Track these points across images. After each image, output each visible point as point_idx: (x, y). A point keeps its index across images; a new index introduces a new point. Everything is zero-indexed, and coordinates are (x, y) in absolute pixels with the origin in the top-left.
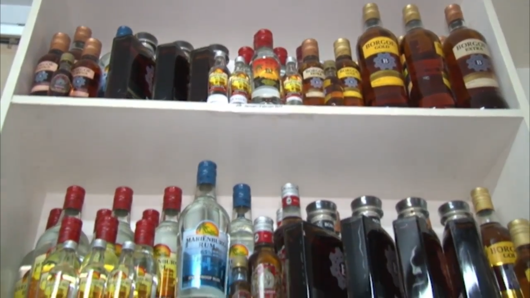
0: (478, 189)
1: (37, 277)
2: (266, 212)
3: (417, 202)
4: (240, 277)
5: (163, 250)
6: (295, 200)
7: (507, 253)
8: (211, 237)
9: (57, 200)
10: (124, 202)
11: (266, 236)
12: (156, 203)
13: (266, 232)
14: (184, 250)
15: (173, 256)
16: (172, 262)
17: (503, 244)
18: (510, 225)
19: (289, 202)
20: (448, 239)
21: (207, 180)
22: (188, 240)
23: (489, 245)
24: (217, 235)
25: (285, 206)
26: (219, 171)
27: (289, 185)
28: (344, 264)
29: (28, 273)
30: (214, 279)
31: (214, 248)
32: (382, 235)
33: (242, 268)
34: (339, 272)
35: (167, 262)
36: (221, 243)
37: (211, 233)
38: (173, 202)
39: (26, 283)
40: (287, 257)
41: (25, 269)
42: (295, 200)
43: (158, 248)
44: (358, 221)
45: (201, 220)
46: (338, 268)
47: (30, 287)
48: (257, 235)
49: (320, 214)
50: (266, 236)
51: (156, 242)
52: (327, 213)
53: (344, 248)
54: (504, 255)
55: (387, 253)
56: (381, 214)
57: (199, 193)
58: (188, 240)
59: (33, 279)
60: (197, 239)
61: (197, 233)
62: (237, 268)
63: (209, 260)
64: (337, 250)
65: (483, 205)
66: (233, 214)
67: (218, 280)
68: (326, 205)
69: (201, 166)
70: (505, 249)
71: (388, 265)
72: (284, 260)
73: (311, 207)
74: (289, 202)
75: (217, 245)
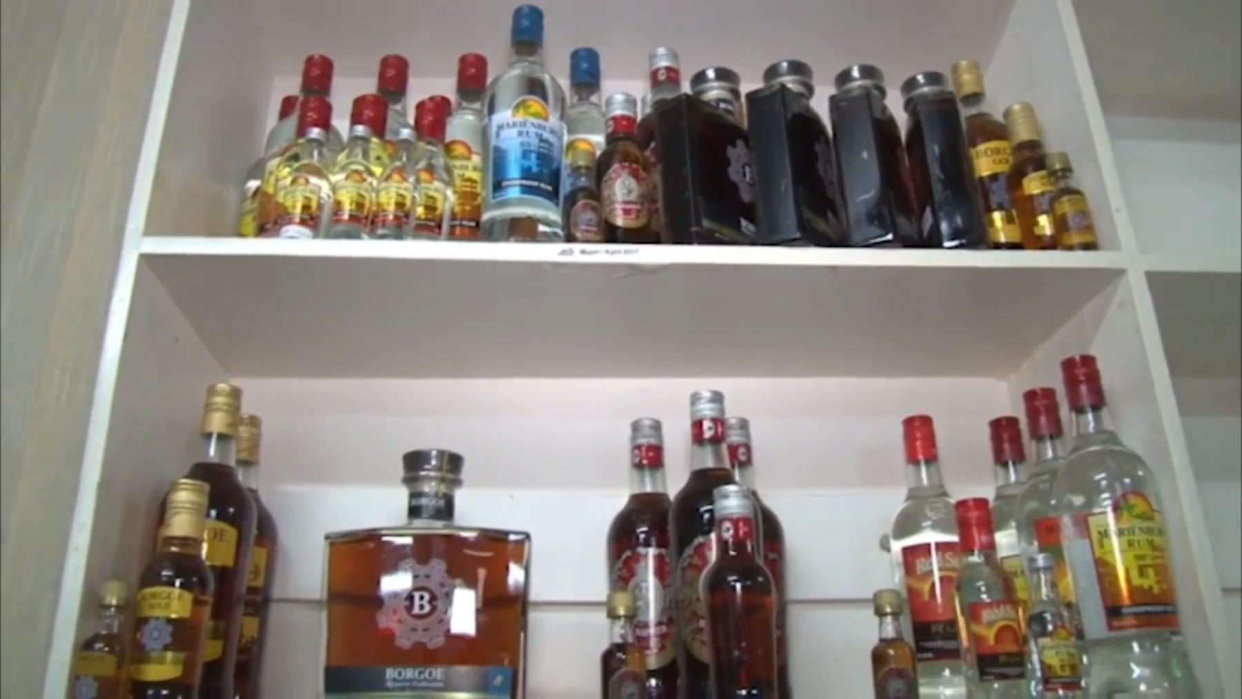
0: (963, 63)
1: (271, 190)
2: (626, 92)
3: (868, 71)
4: (583, 181)
5: (459, 150)
6: (672, 74)
7: (998, 157)
8: (536, 121)
9: (292, 85)
10: (394, 76)
11: (624, 123)
12: (447, 87)
13: (623, 117)
14: (493, 142)
15: (476, 159)
16: (475, 169)
17: (993, 144)
18: (1007, 114)
19: (662, 77)
20: (916, 131)
21: (528, 34)
22: (500, 127)
23: (974, 145)
24: (546, 119)
25: (655, 82)
26: (547, 22)
27: (661, 51)
28: (750, 165)
29: (257, 190)
30: (543, 185)
31: (542, 140)
32: (809, 122)
33: (587, 168)
34: (741, 176)
35: (466, 168)
36: (552, 131)
37: (535, 115)
38: (473, 79)
39: (256, 205)
40: (659, 160)
41: (253, 184)
42: (672, 74)
43: (453, 147)
44: (774, 94)
45: (521, 94)
46: (741, 170)
47: (262, 207)
48: (611, 123)
49: (713, 88)
50: (624, 123)
51: (449, 138)
52: (722, 88)
53: (752, 144)
54: (994, 161)
55: (818, 147)
56: (810, 90)
57: (515, 58)
58: (500, 127)
59: (266, 194)
60: (515, 125)
61: (514, 115)
62: (579, 168)
63: (533, 156)
64: (740, 143)
65: (968, 89)
66: (572, 98)
67: (550, 188)
68: (724, 75)
69: (518, 13)
70: (997, 151)
71: (820, 166)
72: (654, 165)
73: (700, 78)
74: (662, 77)
75: (546, 135)
